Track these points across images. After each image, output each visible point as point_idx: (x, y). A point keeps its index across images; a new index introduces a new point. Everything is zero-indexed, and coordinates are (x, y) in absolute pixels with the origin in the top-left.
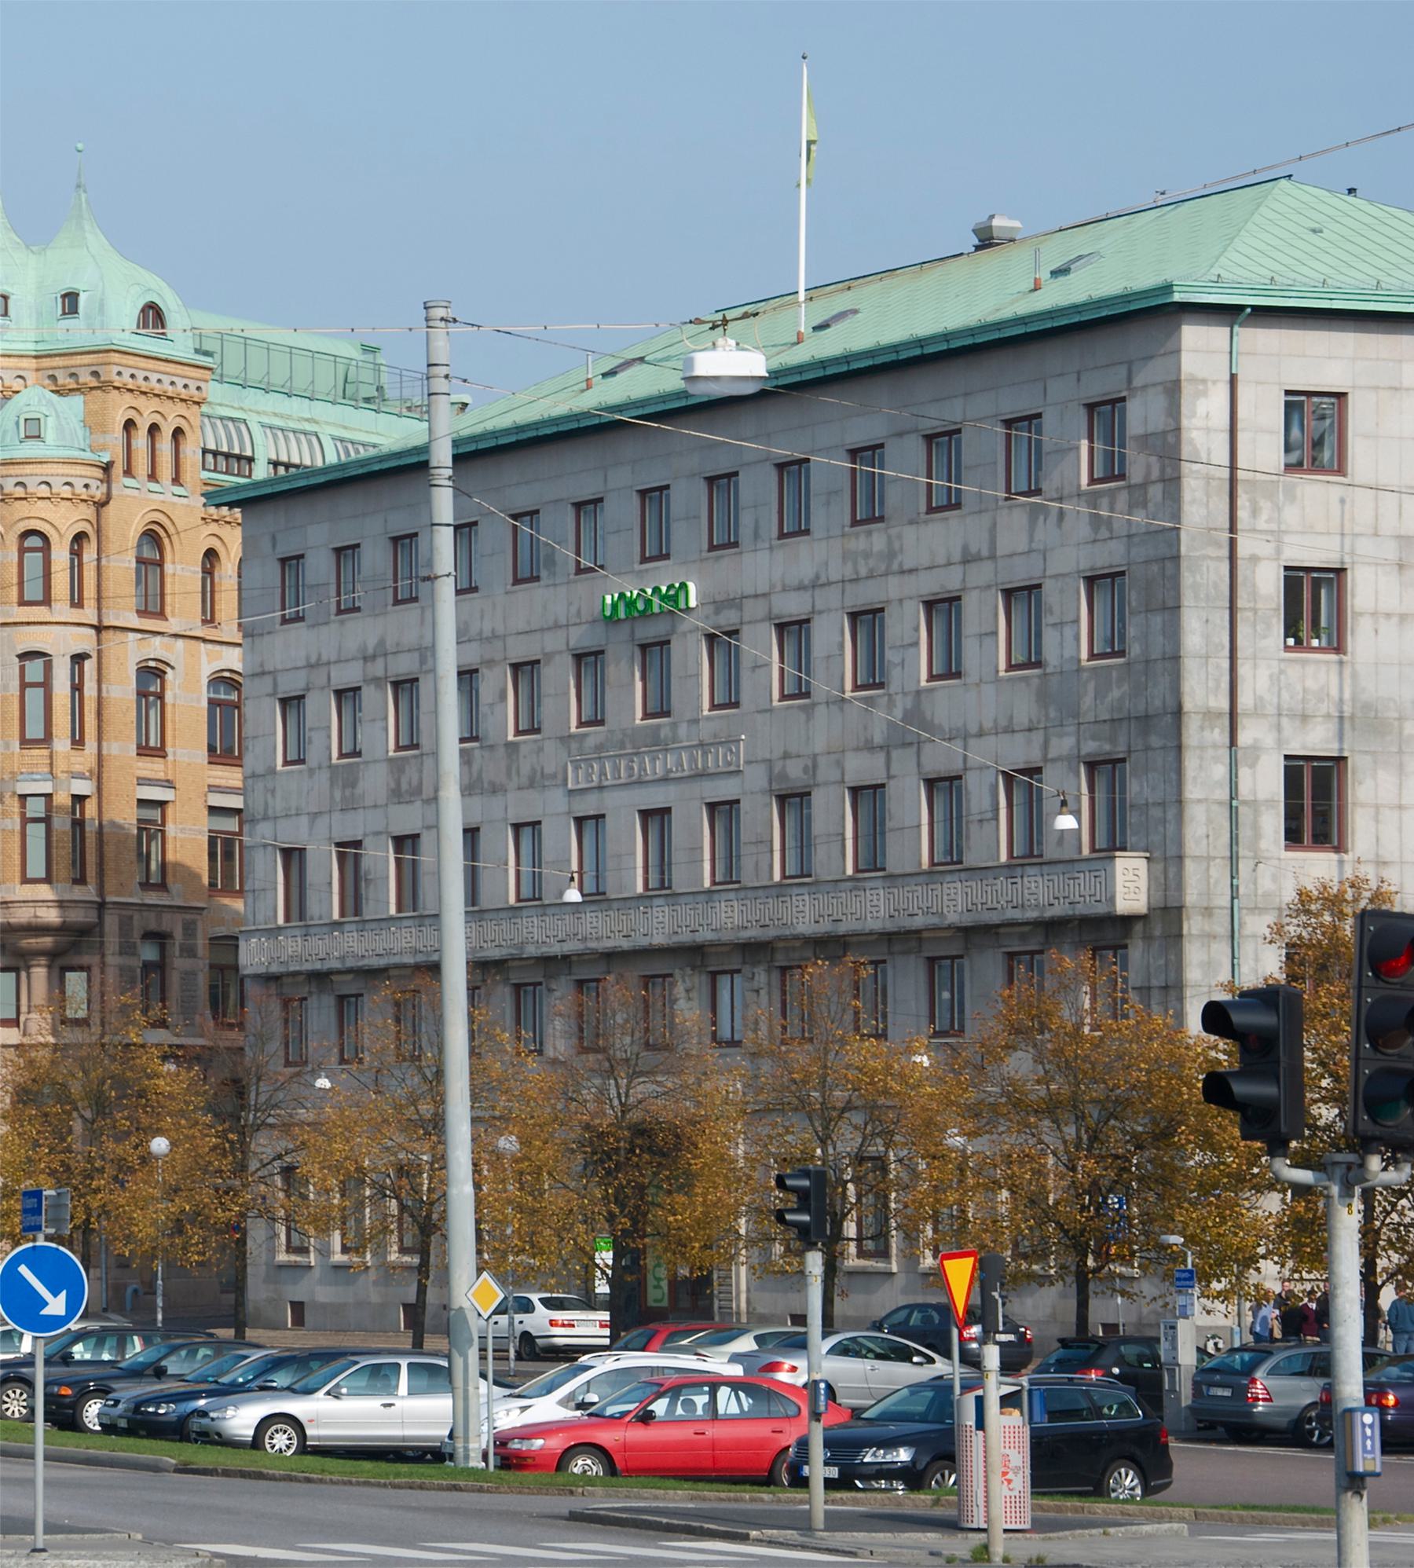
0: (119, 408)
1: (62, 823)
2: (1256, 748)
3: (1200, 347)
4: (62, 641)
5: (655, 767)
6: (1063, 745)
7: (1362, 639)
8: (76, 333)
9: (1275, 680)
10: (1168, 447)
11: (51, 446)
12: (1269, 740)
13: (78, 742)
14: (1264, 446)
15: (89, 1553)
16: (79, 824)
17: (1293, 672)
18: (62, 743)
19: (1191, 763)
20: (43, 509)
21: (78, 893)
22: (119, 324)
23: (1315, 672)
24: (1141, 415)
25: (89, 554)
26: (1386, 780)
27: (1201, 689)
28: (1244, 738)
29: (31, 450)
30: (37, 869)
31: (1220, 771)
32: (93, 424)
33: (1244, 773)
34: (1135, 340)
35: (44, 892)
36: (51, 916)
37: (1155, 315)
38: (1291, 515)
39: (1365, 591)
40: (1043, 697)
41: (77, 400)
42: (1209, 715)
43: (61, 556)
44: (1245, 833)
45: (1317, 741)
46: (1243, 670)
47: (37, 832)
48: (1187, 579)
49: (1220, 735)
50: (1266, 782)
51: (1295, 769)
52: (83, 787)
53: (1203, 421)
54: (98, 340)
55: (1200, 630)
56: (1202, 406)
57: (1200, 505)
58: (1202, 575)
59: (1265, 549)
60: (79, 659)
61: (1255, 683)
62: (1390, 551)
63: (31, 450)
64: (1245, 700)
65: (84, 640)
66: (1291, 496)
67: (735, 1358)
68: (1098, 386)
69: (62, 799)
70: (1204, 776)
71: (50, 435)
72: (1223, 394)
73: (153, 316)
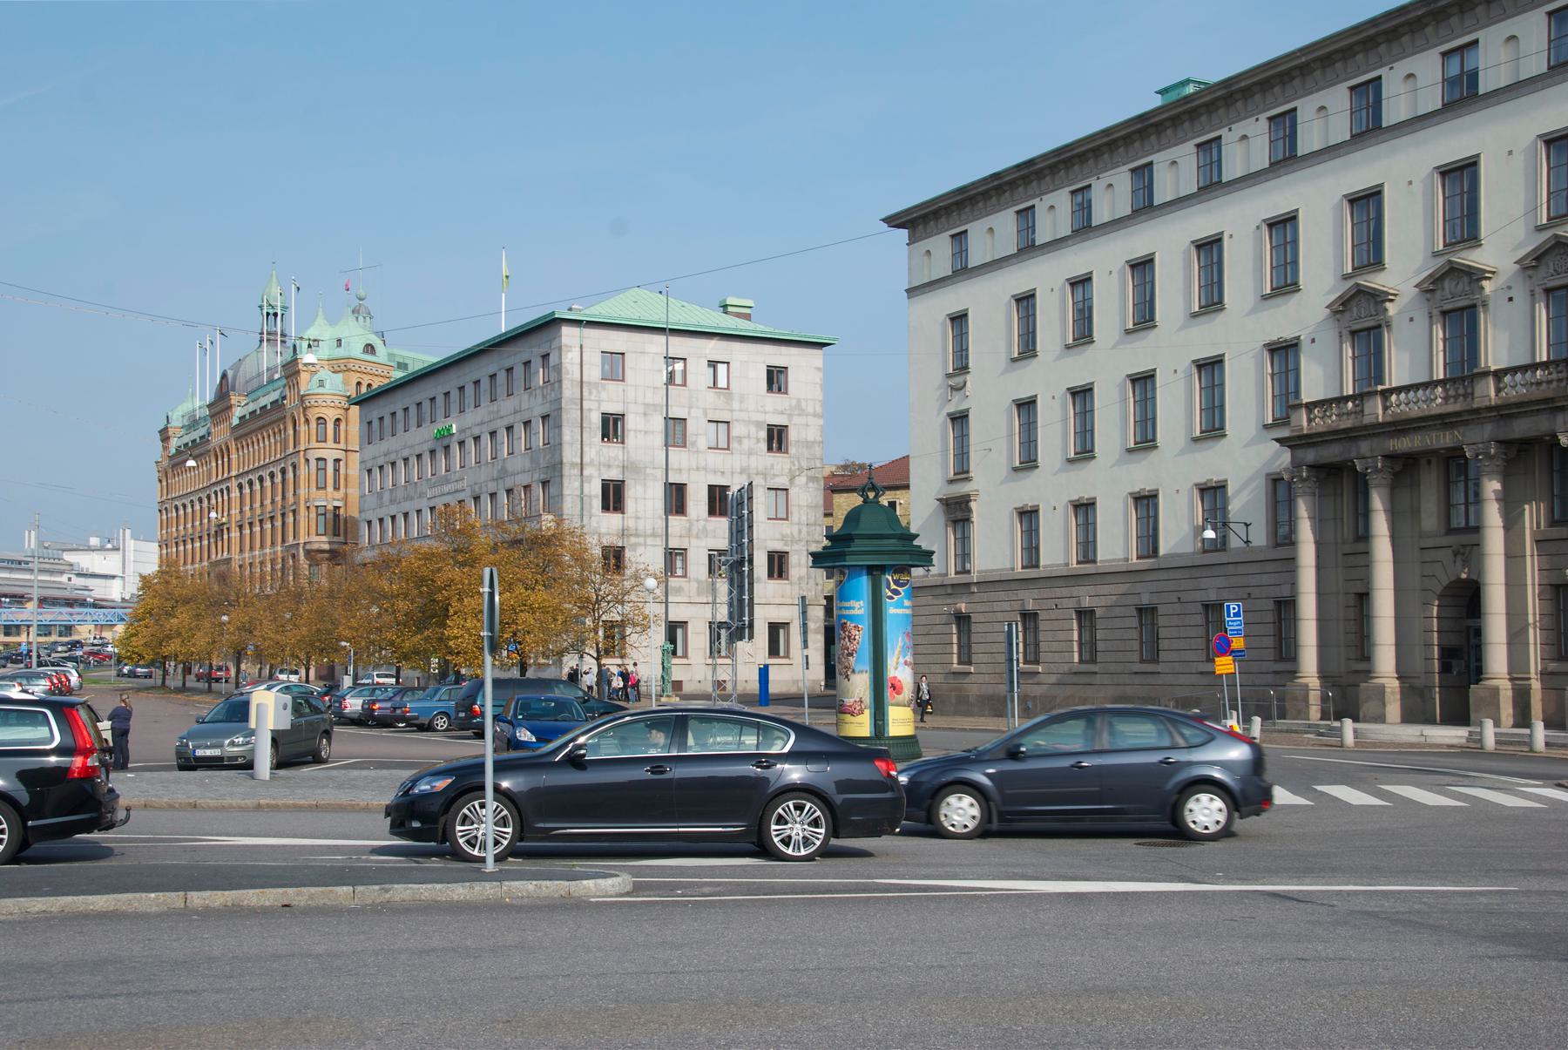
0: (354, 378)
1: (330, 516)
2: (590, 477)
3: (568, 334)
4: (331, 455)
5: (446, 489)
6: (536, 477)
7: (631, 439)
8: (340, 352)
9: (598, 453)
10: (558, 368)
11: (328, 389)
12: (596, 474)
13: (336, 488)
14: (593, 372)
15: (1512, 950)
16: (336, 516)
17: (605, 450)
18: (330, 488)
19: (566, 482)
20: (324, 410)
21: (336, 539)
22: (357, 350)
23: (613, 450)
24: (553, 359)
25: (343, 426)
26: (640, 489)
27: (570, 455)
28: (586, 473)
29: (321, 390)
30: (321, 530)
31: (577, 484)
32: (346, 383)
33: (586, 485)
34: (545, 335)
35: (324, 539)
36: (326, 547)
37: (550, 325)
38: (604, 395)
39: (631, 422)
40: (532, 461)
41: (340, 375)
42: (573, 464)
43: (330, 426)
44: (586, 506)
45: (614, 474)
46: (586, 449)
47: (322, 518)
48: (564, 416)
49: (577, 471)
50: (595, 489)
51: (606, 485)
52: (337, 504)
53: (570, 359)
54: (346, 354)
55: (569, 434)
56: (570, 355)
57: (569, 391)
58: (570, 415)
59: (593, 405)
60: (337, 461)
61: (590, 454)
62: (641, 409)
63: (321, 390)
64: (586, 459)
65: (340, 455)
66: (604, 387)
67: (988, 775)
68: (543, 351)
69: (330, 507)
70: (570, 486)
71: (327, 385)
72: (578, 352)
73: (370, 348)
